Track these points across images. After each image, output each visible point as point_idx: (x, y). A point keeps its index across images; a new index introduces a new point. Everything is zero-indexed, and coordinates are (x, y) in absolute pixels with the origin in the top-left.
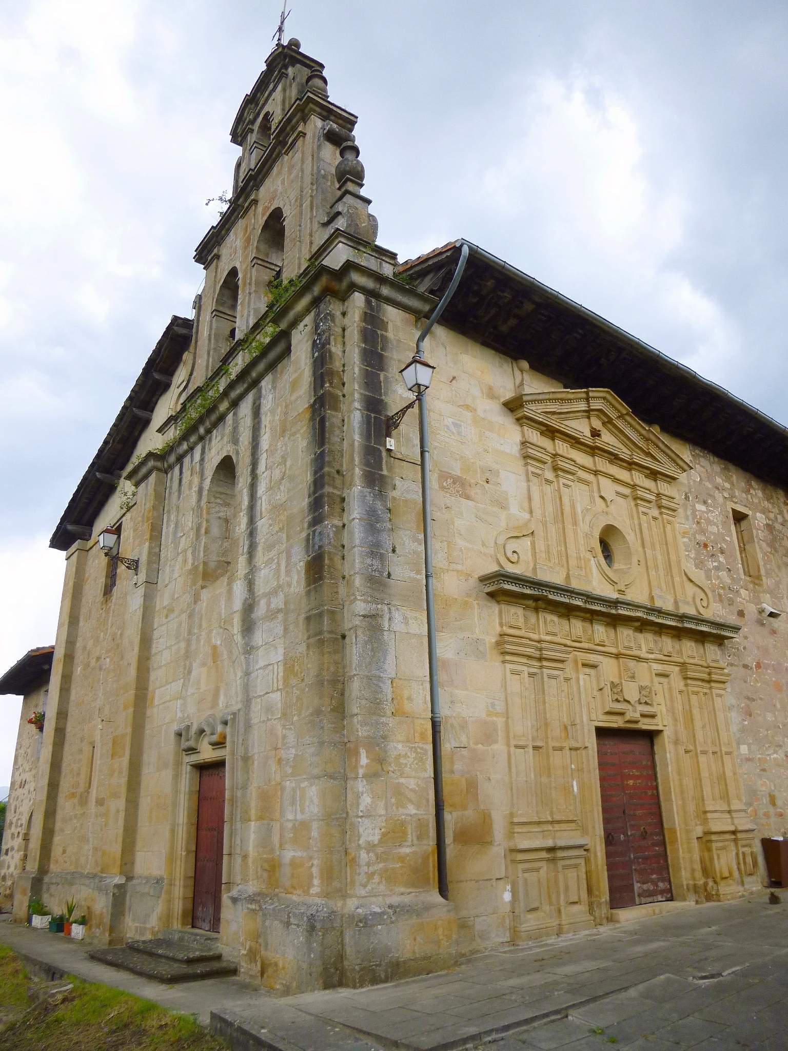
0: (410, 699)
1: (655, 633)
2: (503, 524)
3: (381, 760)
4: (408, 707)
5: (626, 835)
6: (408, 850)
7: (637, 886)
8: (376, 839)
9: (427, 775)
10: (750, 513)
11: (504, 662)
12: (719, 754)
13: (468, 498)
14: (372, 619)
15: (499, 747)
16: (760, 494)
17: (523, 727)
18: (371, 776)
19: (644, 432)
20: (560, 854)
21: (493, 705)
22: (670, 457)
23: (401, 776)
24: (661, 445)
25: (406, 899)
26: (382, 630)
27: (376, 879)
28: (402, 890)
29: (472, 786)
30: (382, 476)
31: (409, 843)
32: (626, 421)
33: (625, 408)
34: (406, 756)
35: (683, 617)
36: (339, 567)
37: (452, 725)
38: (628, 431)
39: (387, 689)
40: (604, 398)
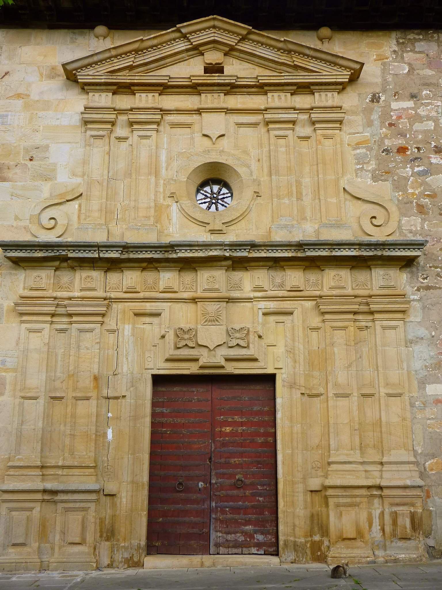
1: (228, 269)
7: (213, 536)
11: (22, 322)
12: (377, 396)
17: (36, 380)
19: (281, 45)
22: (326, 61)
24: (307, 52)
32: (254, 41)
33: (243, 28)
38: (261, 51)
40: (214, 27)
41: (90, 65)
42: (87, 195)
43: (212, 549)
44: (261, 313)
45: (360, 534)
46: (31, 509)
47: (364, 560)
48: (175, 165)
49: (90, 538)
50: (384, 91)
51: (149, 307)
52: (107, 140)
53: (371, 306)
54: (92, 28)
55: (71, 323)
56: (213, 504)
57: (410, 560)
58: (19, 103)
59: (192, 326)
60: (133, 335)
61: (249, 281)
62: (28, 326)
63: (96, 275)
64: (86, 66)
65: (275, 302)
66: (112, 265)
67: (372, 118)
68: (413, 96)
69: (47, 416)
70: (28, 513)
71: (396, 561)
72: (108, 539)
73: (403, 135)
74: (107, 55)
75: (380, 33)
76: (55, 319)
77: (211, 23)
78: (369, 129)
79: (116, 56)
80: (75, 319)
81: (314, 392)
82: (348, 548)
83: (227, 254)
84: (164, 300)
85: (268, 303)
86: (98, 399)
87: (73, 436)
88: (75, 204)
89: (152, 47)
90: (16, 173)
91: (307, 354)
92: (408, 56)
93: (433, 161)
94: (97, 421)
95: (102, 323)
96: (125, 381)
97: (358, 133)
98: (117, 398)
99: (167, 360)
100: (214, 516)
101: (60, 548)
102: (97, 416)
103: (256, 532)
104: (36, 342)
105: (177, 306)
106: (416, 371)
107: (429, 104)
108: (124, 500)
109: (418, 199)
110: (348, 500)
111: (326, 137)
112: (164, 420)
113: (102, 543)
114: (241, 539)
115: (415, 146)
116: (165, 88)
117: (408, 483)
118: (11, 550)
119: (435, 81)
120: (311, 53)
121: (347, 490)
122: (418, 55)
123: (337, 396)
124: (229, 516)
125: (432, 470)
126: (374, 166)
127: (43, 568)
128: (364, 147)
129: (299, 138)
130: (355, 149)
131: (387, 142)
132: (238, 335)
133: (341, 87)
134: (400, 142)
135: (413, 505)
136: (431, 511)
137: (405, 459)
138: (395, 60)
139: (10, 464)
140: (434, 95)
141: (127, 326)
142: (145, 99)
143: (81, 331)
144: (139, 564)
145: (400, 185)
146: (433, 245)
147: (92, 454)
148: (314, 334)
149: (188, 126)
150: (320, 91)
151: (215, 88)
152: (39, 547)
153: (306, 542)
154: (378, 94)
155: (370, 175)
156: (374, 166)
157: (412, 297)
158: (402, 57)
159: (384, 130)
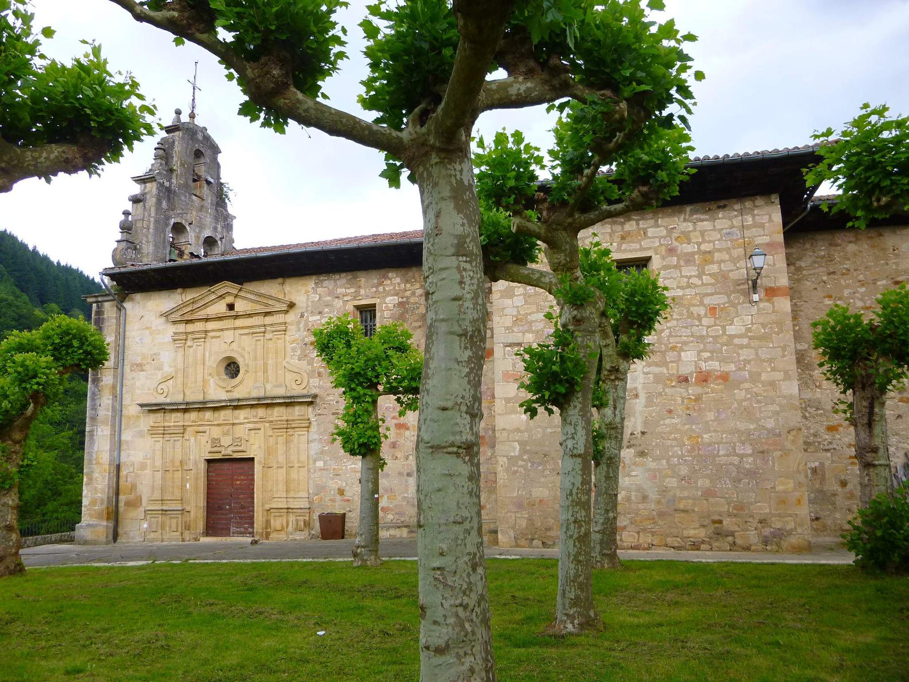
2: (160, 377)
4: (101, 461)
10: (376, 301)
13: (143, 370)
14: (91, 431)
15: (148, 472)
16: (398, 280)
17: (158, 463)
18: (88, 484)
29: (133, 487)
36: (627, 170)
39: (94, 456)
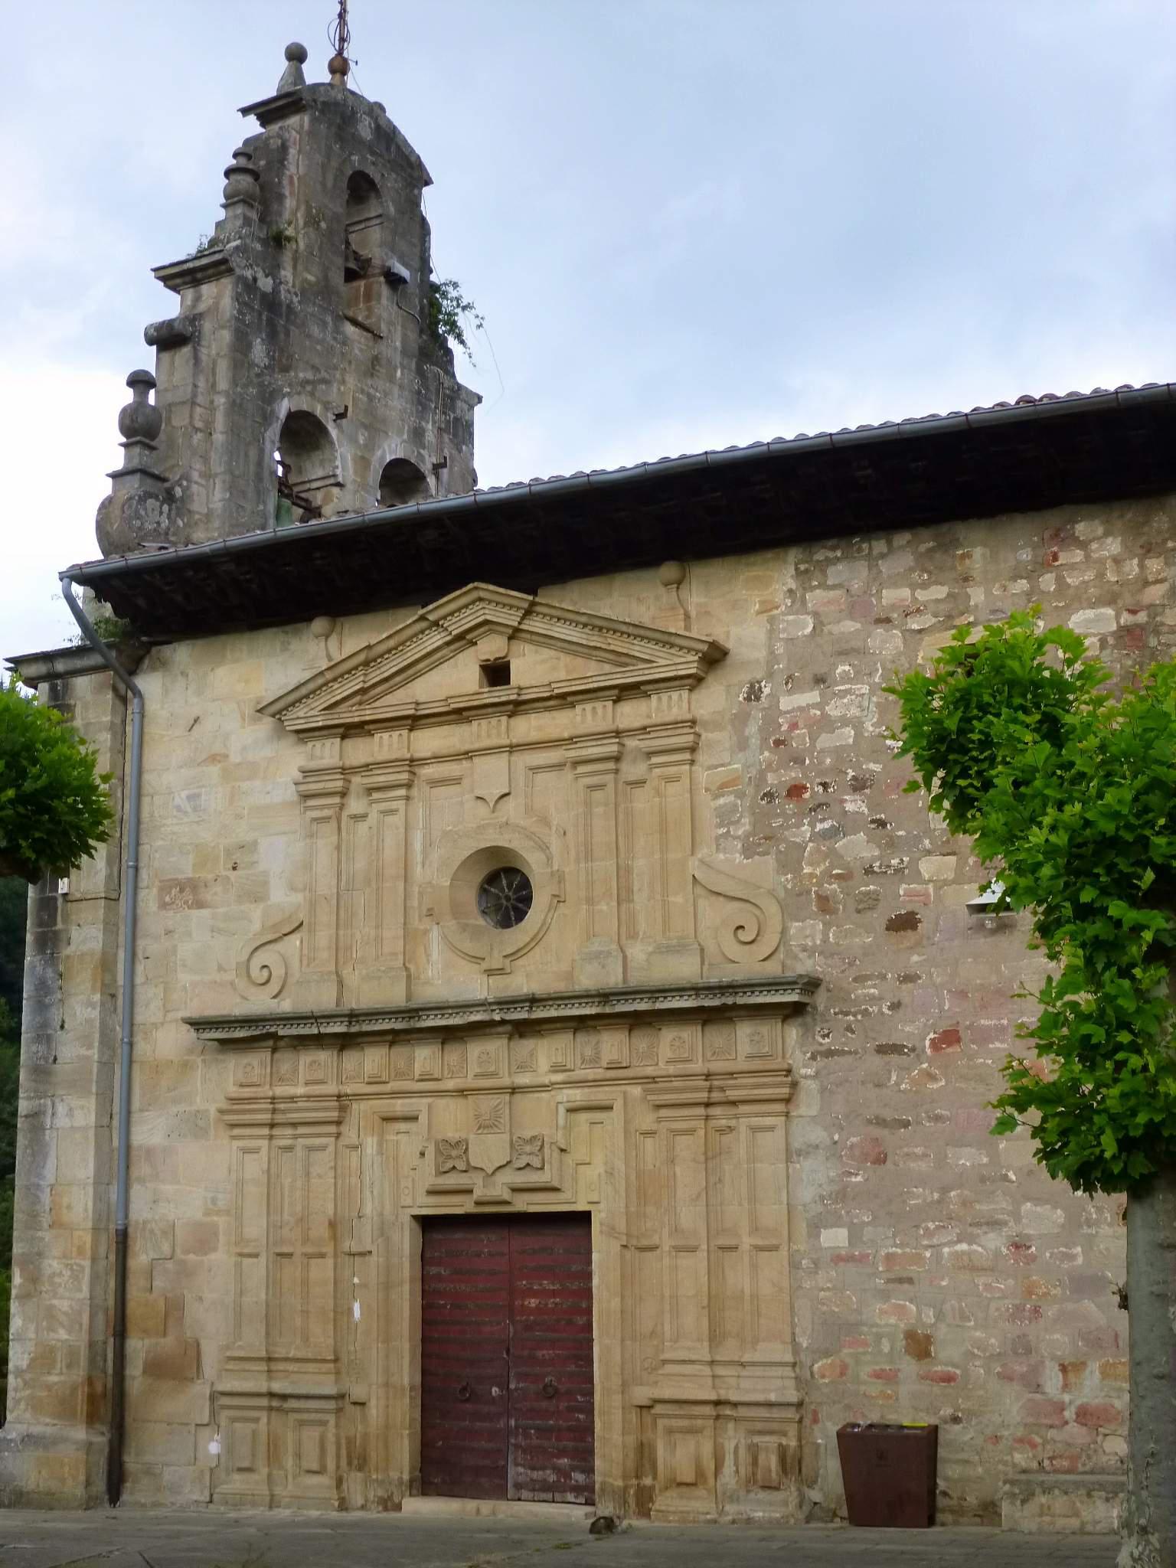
0: (69, 1207)
3: (34, 1279)
5: (504, 1385)
6: (54, 1379)
7: (512, 1471)
8: (24, 1364)
9: (81, 1296)
11: (234, 1138)
17: (255, 1228)
20: (292, 1404)
21: (214, 1201)
23: (55, 1296)
25: (49, 1430)
26: (44, 1129)
27: (22, 1406)
28: (48, 1420)
29: (174, 1309)
30: (56, 933)
31: (58, 1371)
34: (60, 1274)
35: (353, 1016)
37: (152, 1231)
39: (46, 1198)
40: (480, 599)
41: (299, 701)
42: (310, 924)
43: (511, 1492)
44: (562, 1110)
45: (700, 1473)
46: (257, 1420)
47: (702, 1518)
48: (435, 855)
49: (331, 1465)
50: (770, 675)
51: (400, 1106)
52: (334, 824)
53: (728, 1093)
54: (309, 619)
55: (295, 1137)
56: (513, 1422)
57: (770, 1521)
58: (214, 770)
59: (464, 1136)
60: (380, 1153)
61: (545, 1055)
62: (241, 1143)
63: (324, 1057)
64: (293, 704)
65: (586, 1090)
66: (345, 1042)
67: (747, 734)
68: (820, 680)
69: (273, 1283)
70: (253, 1426)
71: (749, 1521)
72: (360, 1469)
73: (799, 761)
74: (320, 681)
75: (769, 555)
76: (276, 1132)
77: (474, 595)
78: (740, 755)
79: (335, 680)
80: (301, 1130)
81: (645, 1242)
82: (682, 1498)
83: (497, 1018)
84: (421, 1093)
85: (571, 1092)
86: (335, 1256)
87: (305, 1313)
88: (295, 940)
89: (389, 651)
90: (215, 894)
91: (633, 1177)
92: (816, 598)
93: (850, 807)
94: (335, 1291)
95: (338, 1135)
96: (369, 1228)
97: (722, 765)
98: (362, 1254)
99: (430, 1193)
100: (513, 1441)
101: (294, 1477)
102: (335, 1283)
103: (574, 1469)
104: (254, 1167)
105: (441, 1103)
106: (804, 1206)
107: (847, 692)
108: (374, 1412)
109: (820, 884)
110: (685, 1423)
111: (670, 780)
112: (441, 1286)
113: (353, 1474)
114: (552, 1478)
115: (818, 780)
116: (415, 721)
117: (773, 1397)
118: (237, 1477)
119: (856, 643)
120: (631, 630)
121: (685, 1406)
122: (832, 594)
123: (678, 1249)
124: (535, 1442)
125: (823, 1377)
126: (747, 827)
127: (273, 1503)
128: (731, 793)
129: (628, 783)
130: (716, 797)
131: (771, 778)
132: (528, 1148)
133: (695, 682)
134: (793, 775)
135: (784, 1434)
136: (819, 1445)
137: (777, 1358)
138: (790, 611)
139: (228, 1354)
140: (857, 673)
141: (369, 1140)
142: (387, 745)
143: (310, 1149)
144: (398, 1507)
145: (790, 862)
146: (843, 971)
147: (331, 1341)
148: (649, 1141)
149: (457, 781)
150: (658, 691)
151: (490, 710)
152: (269, 1475)
153: (626, 1488)
154: (759, 682)
155: (740, 846)
156: (747, 827)
157: (803, 1071)
158: (804, 602)
159: (766, 754)
